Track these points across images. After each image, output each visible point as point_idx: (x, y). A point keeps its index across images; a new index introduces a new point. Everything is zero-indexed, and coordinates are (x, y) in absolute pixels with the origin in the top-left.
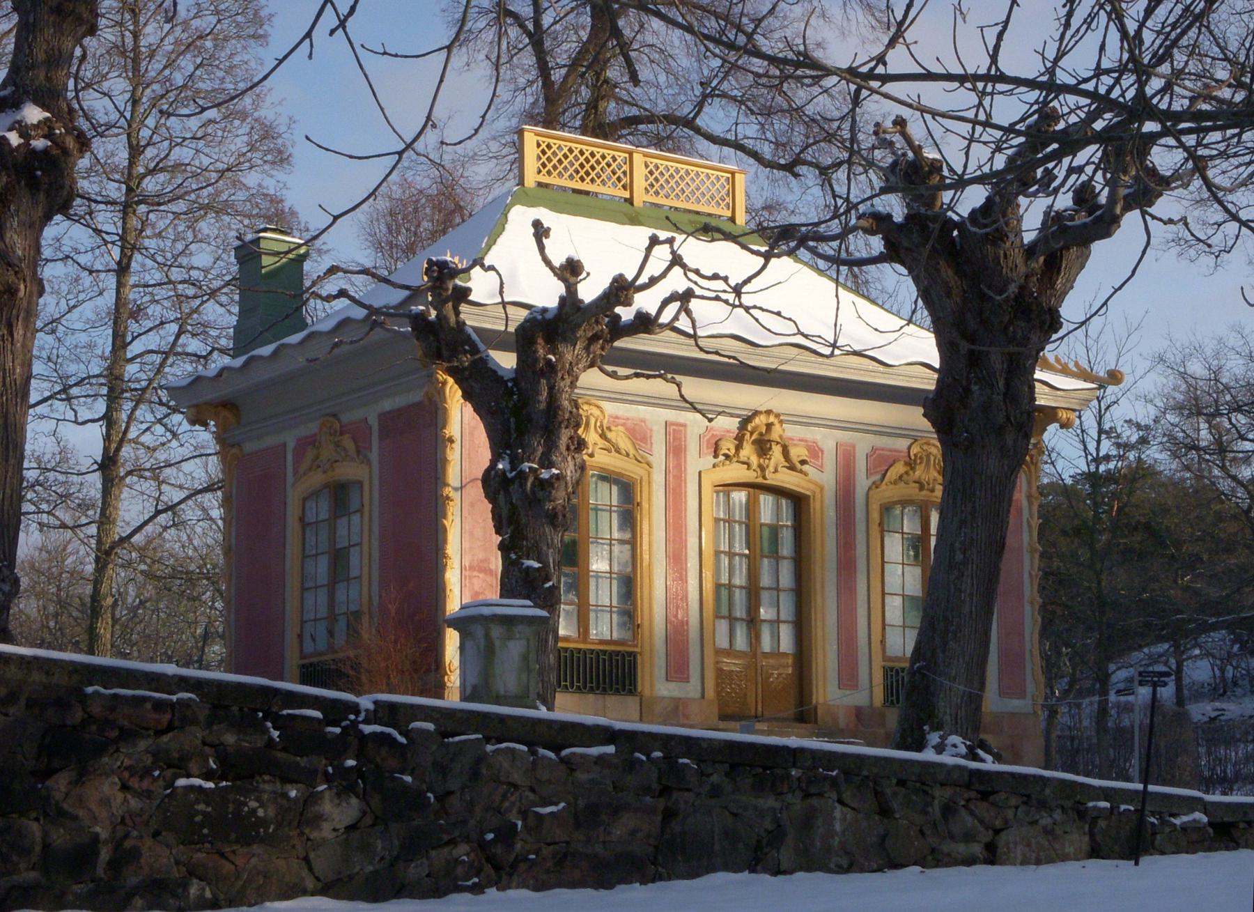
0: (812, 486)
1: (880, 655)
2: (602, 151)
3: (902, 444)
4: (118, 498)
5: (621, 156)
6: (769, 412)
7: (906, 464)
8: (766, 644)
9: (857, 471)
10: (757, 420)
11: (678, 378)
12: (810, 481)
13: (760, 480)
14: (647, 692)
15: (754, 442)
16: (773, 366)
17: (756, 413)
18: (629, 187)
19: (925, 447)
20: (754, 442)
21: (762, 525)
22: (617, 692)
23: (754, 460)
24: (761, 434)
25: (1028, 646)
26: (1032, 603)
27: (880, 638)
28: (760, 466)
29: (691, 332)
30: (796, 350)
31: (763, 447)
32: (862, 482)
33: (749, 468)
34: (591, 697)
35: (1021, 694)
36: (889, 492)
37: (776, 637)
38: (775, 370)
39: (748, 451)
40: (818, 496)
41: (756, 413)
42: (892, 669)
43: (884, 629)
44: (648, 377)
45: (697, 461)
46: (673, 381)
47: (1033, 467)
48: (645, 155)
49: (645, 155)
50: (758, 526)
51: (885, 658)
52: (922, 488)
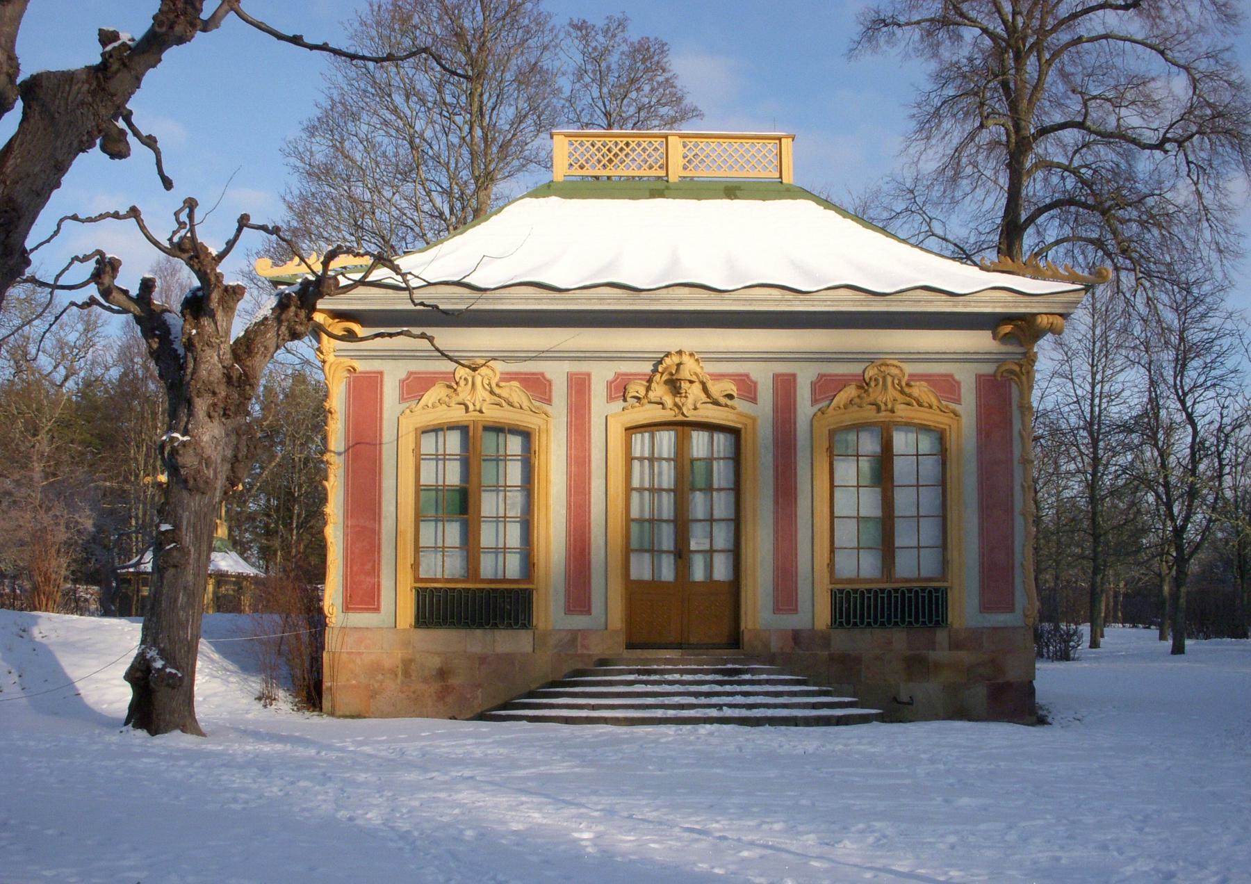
0: (744, 420)
1: (827, 575)
2: (625, 140)
3: (856, 369)
4: (907, 432)
5: (657, 142)
6: (680, 353)
7: (860, 387)
8: (698, 574)
9: (799, 399)
10: (668, 361)
11: (429, 331)
12: (740, 414)
13: (680, 418)
14: (541, 626)
15: (666, 382)
16: (463, 307)
17: (668, 354)
18: (666, 166)
19: (883, 368)
20: (666, 382)
21: (692, 461)
22: (510, 626)
23: (668, 400)
24: (671, 374)
25: (1018, 557)
26: (1024, 515)
27: (826, 561)
28: (676, 405)
29: (403, 285)
30: (687, 290)
31: (674, 385)
32: (805, 408)
33: (664, 408)
34: (479, 632)
35: (1011, 609)
36: (834, 418)
37: (709, 567)
38: (467, 310)
39: (659, 391)
40: (750, 427)
41: (668, 354)
42: (841, 591)
43: (832, 551)
44: (391, 335)
45: (600, 406)
46: (423, 336)
47: (1024, 378)
48: (681, 136)
49: (681, 136)
50: (687, 462)
51: (833, 580)
52: (879, 410)
